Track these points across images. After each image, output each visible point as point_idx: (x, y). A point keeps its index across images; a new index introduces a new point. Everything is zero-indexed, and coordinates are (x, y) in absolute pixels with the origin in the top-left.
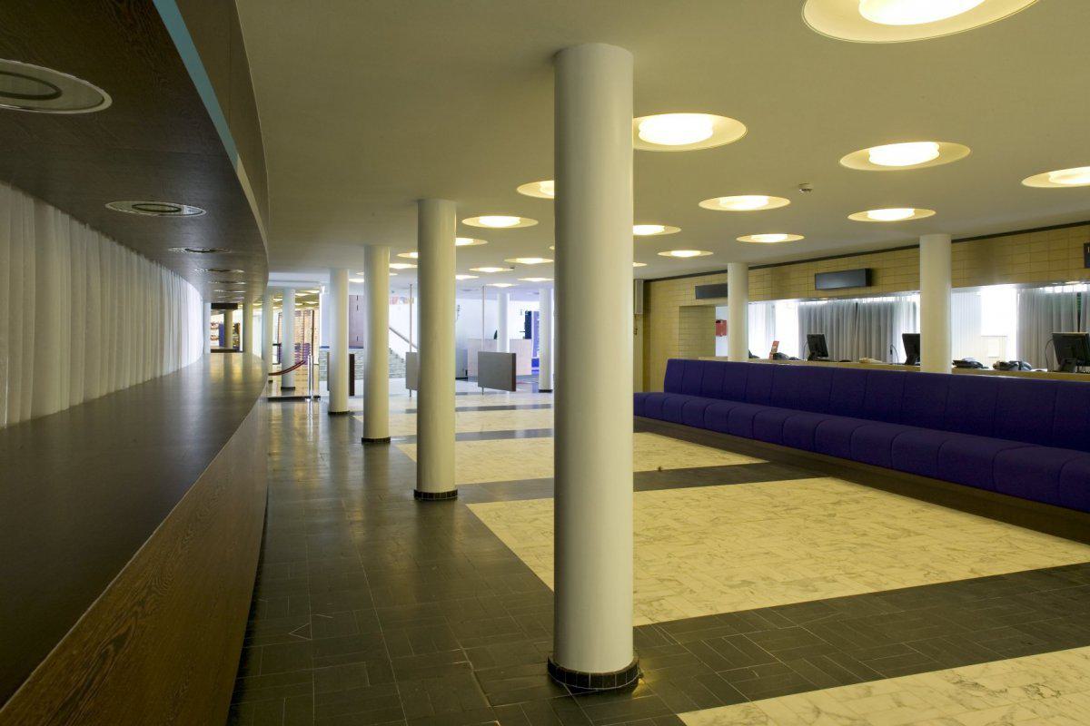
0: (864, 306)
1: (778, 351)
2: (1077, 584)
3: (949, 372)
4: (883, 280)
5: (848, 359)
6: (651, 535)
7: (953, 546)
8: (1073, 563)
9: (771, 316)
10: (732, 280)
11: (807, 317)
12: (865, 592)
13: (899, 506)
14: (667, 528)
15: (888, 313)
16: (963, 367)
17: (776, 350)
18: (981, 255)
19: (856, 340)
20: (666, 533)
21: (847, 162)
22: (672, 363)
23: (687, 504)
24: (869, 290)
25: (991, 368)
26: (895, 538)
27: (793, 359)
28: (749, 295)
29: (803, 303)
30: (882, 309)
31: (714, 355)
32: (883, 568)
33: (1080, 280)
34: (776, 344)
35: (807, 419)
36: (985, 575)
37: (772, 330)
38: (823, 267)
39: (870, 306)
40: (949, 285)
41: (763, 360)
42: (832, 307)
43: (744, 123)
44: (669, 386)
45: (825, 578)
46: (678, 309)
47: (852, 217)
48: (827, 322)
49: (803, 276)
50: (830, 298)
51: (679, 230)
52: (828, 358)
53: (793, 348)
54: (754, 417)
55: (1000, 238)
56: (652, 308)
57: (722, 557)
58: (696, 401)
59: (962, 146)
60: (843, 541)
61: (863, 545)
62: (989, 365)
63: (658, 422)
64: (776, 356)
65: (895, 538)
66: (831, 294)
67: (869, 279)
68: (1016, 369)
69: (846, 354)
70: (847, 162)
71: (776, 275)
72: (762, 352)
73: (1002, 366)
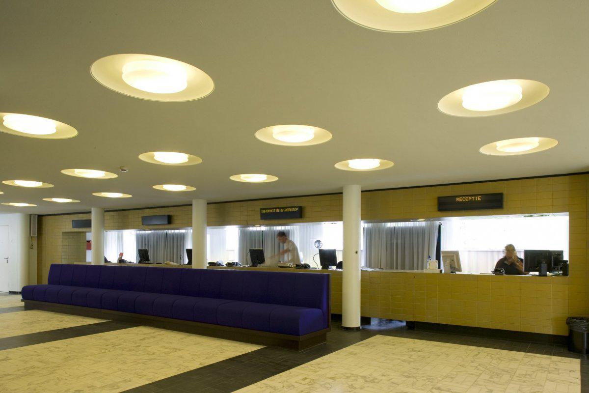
0: (170, 234)
1: (123, 258)
2: (244, 362)
3: (206, 268)
4: (176, 221)
5: (160, 262)
6: (20, 373)
7: (195, 354)
8: (245, 353)
9: (120, 239)
10: (94, 218)
11: (141, 240)
12: (145, 384)
13: (175, 337)
14: (33, 367)
15: (182, 238)
16: (212, 265)
17: (121, 258)
18: (222, 211)
19: (380, 255)
20: (31, 370)
21: (143, 157)
22: (53, 266)
23: (51, 351)
24: (171, 226)
25: (225, 265)
26: (167, 354)
27: (130, 262)
28: (105, 226)
29: (138, 232)
30: (144, 237)
31: (85, 261)
32: (158, 370)
33: (263, 225)
34: (121, 254)
35: (114, 293)
36: (206, 365)
37: (120, 247)
38: (147, 213)
39: (173, 234)
40: (206, 225)
41: (114, 264)
42: (154, 234)
43: (332, 133)
44: (51, 280)
45: (125, 380)
46: (61, 234)
47: (155, 187)
48: (151, 243)
49: (137, 217)
50: (150, 230)
51: (195, 189)
52: (150, 262)
53: (131, 257)
54: (72, 294)
55: (229, 204)
56: (44, 232)
57: (66, 379)
58: (69, 289)
59: (199, 158)
60: (141, 359)
61: (150, 360)
62: (224, 264)
63: (43, 303)
64: (121, 261)
65: (167, 354)
66: (152, 227)
67: (170, 220)
68: (235, 266)
69: (161, 259)
70: (143, 157)
71: (121, 216)
72: (113, 259)
73: (229, 265)
